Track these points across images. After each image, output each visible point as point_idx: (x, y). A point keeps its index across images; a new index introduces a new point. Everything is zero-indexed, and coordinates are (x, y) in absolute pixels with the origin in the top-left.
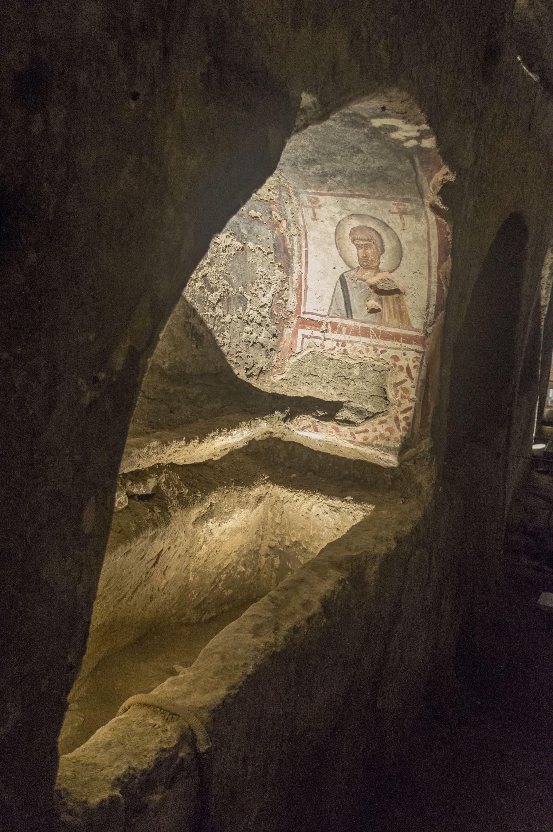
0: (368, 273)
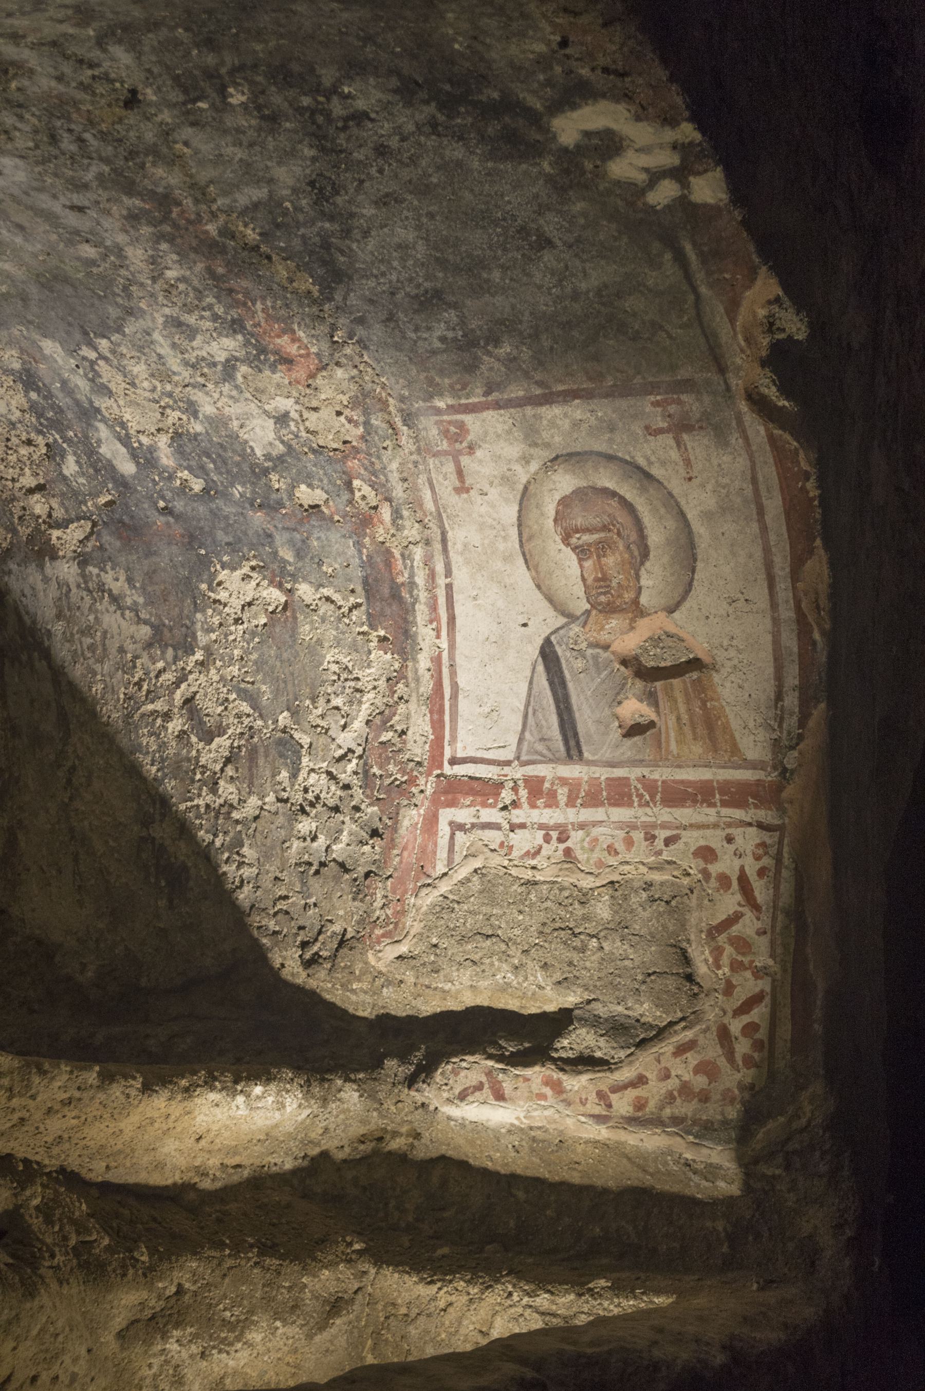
0: (614, 622)
